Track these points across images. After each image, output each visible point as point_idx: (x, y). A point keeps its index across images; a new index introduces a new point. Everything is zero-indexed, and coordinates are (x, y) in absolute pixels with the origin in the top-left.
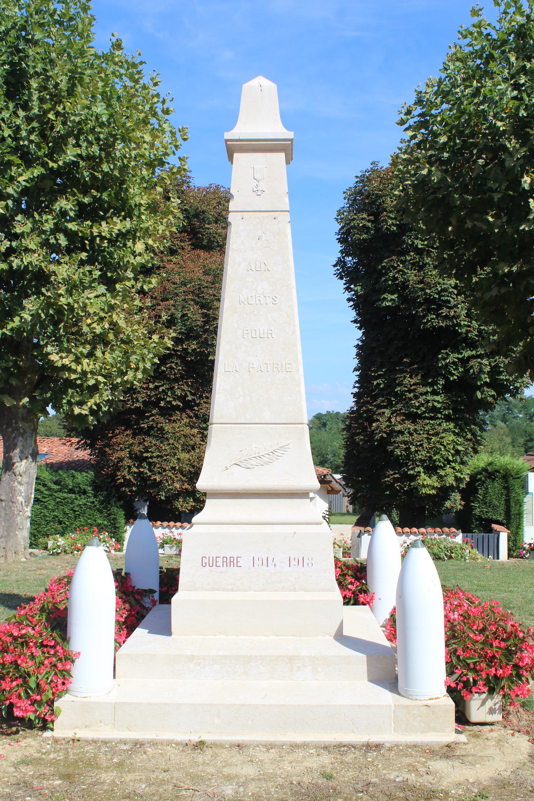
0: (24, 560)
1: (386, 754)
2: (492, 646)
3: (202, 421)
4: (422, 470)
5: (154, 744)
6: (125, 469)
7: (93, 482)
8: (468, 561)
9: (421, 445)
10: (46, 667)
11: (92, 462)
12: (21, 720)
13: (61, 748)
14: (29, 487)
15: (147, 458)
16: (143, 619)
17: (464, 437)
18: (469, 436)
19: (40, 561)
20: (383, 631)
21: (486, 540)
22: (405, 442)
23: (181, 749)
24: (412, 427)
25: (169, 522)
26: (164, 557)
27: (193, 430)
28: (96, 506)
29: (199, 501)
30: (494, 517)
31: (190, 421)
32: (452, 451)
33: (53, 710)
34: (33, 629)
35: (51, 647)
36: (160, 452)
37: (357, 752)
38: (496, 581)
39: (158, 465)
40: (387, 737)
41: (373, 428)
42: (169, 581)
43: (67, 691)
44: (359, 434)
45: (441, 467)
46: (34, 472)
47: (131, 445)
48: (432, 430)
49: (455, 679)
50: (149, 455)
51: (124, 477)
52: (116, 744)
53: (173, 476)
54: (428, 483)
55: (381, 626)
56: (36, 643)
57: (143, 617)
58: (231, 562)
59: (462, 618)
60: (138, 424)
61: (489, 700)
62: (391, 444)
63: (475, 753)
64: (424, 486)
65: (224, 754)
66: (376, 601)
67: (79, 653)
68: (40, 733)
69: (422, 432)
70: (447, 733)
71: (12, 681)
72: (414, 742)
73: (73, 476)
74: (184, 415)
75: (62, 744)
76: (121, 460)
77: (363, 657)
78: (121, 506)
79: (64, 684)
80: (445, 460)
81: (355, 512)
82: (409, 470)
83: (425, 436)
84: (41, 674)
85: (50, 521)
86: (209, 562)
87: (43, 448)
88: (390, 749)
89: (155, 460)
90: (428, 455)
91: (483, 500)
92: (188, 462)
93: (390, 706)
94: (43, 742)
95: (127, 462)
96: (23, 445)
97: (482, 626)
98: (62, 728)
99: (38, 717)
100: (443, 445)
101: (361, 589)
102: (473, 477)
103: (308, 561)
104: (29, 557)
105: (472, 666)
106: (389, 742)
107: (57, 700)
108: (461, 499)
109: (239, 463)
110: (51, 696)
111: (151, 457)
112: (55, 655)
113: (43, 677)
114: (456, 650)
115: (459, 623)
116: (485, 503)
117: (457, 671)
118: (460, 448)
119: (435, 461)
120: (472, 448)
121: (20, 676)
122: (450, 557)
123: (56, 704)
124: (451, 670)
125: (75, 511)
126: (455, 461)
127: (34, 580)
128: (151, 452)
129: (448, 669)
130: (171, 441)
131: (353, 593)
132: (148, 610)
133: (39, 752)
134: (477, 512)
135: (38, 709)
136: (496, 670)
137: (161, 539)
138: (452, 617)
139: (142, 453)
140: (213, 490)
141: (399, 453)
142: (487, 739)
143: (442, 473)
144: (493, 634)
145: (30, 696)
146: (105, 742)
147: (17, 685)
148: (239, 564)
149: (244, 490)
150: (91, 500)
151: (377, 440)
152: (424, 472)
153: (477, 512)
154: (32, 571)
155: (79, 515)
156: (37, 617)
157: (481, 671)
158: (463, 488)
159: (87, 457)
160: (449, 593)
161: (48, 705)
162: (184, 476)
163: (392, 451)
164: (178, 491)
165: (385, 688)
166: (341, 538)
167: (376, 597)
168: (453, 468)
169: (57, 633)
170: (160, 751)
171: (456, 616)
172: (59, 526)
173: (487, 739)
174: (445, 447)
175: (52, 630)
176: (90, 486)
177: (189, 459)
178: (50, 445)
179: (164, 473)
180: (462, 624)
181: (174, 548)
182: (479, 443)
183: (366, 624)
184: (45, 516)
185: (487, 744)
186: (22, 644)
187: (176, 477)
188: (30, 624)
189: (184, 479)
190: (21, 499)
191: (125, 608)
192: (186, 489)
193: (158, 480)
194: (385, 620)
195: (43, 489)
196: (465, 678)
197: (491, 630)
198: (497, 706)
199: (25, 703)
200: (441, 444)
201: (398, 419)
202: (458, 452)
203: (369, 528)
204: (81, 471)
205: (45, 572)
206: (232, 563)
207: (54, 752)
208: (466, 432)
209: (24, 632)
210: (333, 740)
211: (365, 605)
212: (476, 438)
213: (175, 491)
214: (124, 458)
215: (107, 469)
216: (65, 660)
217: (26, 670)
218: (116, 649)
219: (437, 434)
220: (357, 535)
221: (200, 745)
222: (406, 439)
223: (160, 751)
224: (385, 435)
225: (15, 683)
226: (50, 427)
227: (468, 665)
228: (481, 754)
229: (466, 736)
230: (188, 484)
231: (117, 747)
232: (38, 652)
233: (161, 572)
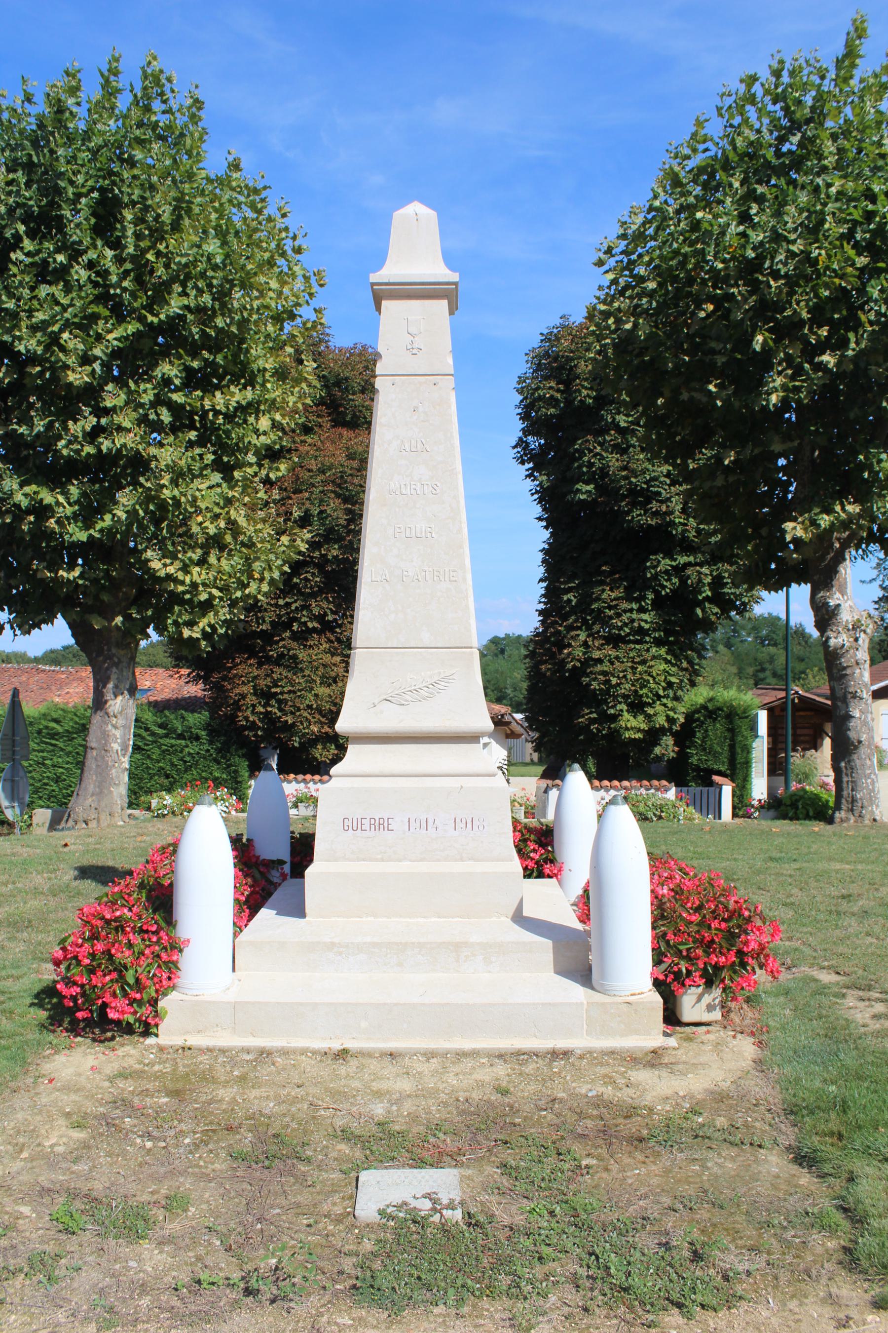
2: (709, 927)
4: (625, 708)
5: (285, 1052)
7: (208, 725)
9: (625, 676)
12: (118, 1023)
18: (685, 664)
19: (142, 825)
22: (604, 673)
24: (613, 653)
25: (304, 774)
29: (339, 745)
30: (715, 767)
32: (663, 684)
34: (130, 910)
35: (153, 933)
37: (540, 1061)
39: (290, 703)
40: (578, 1042)
42: (303, 849)
43: (174, 988)
44: (545, 662)
45: (649, 705)
47: (255, 678)
50: (278, 690)
51: (246, 718)
53: (309, 717)
54: (632, 725)
56: (134, 928)
57: (270, 894)
58: (380, 825)
64: (627, 729)
65: (373, 1065)
66: (565, 873)
67: (188, 941)
68: (141, 1040)
70: (652, 1035)
71: (105, 975)
73: (183, 717)
75: (169, 1053)
76: (243, 696)
77: (548, 943)
78: (244, 756)
79: (169, 978)
82: (609, 708)
83: (630, 664)
85: (154, 775)
86: (351, 825)
88: (581, 1057)
89: (286, 696)
93: (582, 1004)
95: (251, 699)
97: (697, 903)
98: (168, 1034)
102: (689, 717)
104: (127, 820)
105: (684, 953)
106: (580, 1048)
110: (154, 994)
111: (282, 693)
112: (158, 942)
114: (664, 935)
116: (704, 749)
118: (673, 679)
119: (641, 696)
122: (660, 818)
125: (185, 762)
130: (307, 672)
131: (537, 863)
132: (276, 886)
139: (270, 687)
143: (650, 711)
146: (223, 1051)
147: (111, 980)
150: (206, 747)
151: (569, 671)
152: (628, 711)
153: (694, 760)
156: (135, 896)
159: (200, 694)
160: (657, 862)
166: (522, 794)
167: (566, 868)
168: (665, 705)
171: (665, 891)
175: (154, 912)
182: (697, 673)
183: (552, 901)
184: (148, 768)
186: (116, 929)
189: (323, 720)
190: (116, 746)
192: (326, 733)
193: (290, 722)
195: (144, 734)
196: (676, 969)
198: (717, 1001)
199: (121, 1003)
202: (670, 685)
203: (558, 782)
207: (160, 1063)
209: (118, 913)
218: (235, 935)
219: (644, 662)
221: (343, 1054)
224: (578, 664)
225: (108, 978)
227: (681, 951)
228: (695, 1061)
232: (137, 939)
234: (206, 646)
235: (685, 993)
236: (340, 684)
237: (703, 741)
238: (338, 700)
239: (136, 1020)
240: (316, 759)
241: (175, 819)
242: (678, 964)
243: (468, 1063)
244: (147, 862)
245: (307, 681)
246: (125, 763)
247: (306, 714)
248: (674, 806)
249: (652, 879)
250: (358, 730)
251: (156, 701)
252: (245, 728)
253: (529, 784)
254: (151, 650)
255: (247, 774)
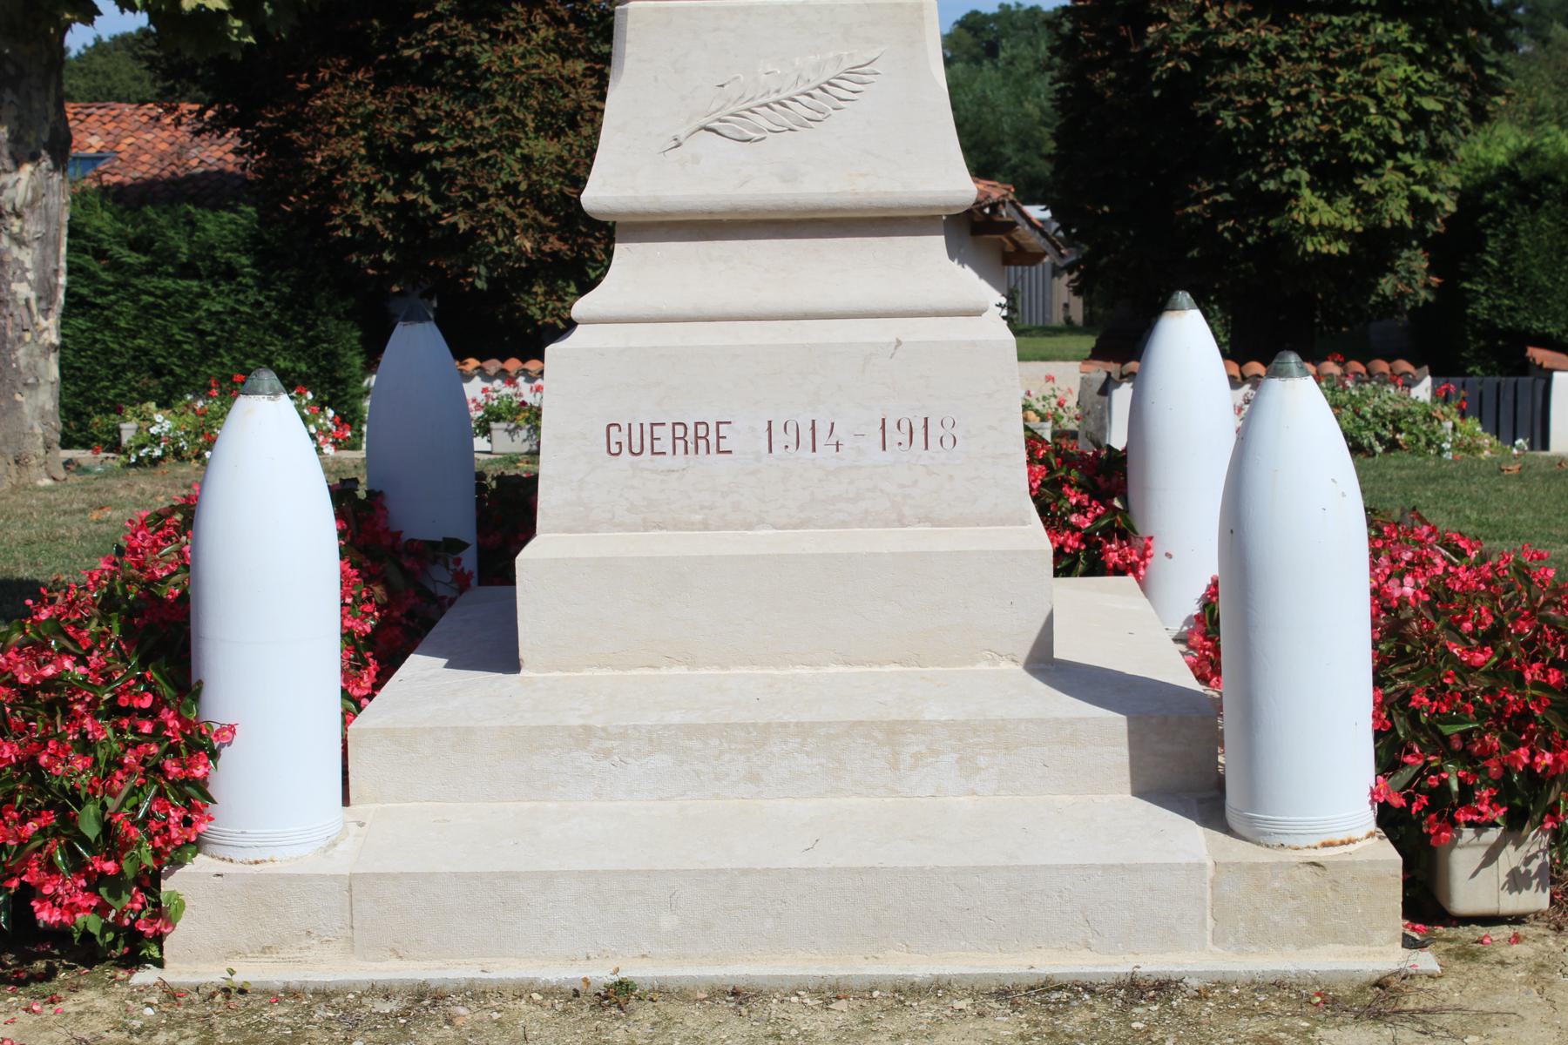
0: (48, 482)
1: (1188, 1010)
2: (1519, 681)
3: (597, 35)
4: (1305, 176)
5: (475, 993)
6: (354, 195)
7: (256, 239)
8: (1448, 456)
9: (1304, 96)
10: (131, 773)
11: (251, 176)
12: (59, 935)
13: (188, 1016)
14: (49, 250)
15: (426, 156)
16: (428, 629)
17: (1443, 69)
18: (1459, 65)
19: (99, 484)
20: (1183, 654)
21: (1507, 398)
22: (1248, 88)
23: (559, 1007)
24: (1272, 37)
26: (491, 462)
27: (569, 63)
28: (268, 315)
29: (584, 248)
30: (1535, 325)
31: (557, 35)
32: (1403, 115)
33: (158, 905)
34: (81, 660)
35: (143, 713)
36: (467, 138)
37: (1101, 1006)
38: (1537, 511)
39: (461, 180)
40: (1192, 960)
41: (1148, 43)
42: (509, 510)
43: (198, 845)
44: (1103, 64)
45: (1367, 169)
46: (60, 204)
47: (372, 117)
48: (1340, 45)
49: (1403, 783)
50: (431, 147)
51: (352, 221)
52: (359, 997)
53: (510, 214)
54: (1322, 218)
55: (1176, 640)
56: (92, 705)
57: (429, 624)
58: (700, 438)
59: (1427, 598)
60: (392, 49)
61: (1510, 848)
62: (1206, 94)
63: (1465, 1004)
64: (1310, 230)
65: (693, 1018)
66: (1157, 562)
67: (232, 729)
68: (121, 974)
69: (1305, 55)
70: (1379, 948)
71: (24, 820)
72: (1275, 973)
73: (191, 223)
74: (538, 18)
75: (191, 1003)
76: (340, 165)
77: (1117, 722)
78: (349, 315)
79: (187, 822)
80: (1379, 144)
81: (1089, 325)
82: (1264, 177)
83: (1315, 66)
84: (113, 795)
85: (124, 368)
86: (627, 441)
87: (88, 139)
88: (1201, 996)
89: (451, 162)
90: (1325, 128)
91: (1498, 271)
92: (556, 168)
93: (1202, 866)
94: (133, 999)
95: (361, 172)
96: (18, 118)
97: (1489, 621)
98: (192, 957)
99: (115, 927)
100: (1374, 96)
101: (1110, 525)
102: (1469, 198)
103: (941, 432)
104: (62, 474)
105: (1457, 745)
106: (1198, 975)
107: (170, 873)
108: (1430, 271)
109: (715, 125)
110: (149, 861)
111: (440, 155)
112: (156, 735)
113: (123, 804)
114: (1406, 696)
115: (1417, 611)
116: (1507, 281)
117: (1409, 759)
118: (1429, 104)
119: (1347, 147)
120: (1466, 104)
121: (50, 805)
122: (1392, 445)
123: (167, 886)
124: (1389, 754)
126: (1411, 148)
127: (83, 537)
128: (436, 137)
129: (1382, 753)
130: (501, 102)
131: (1087, 538)
132: (443, 605)
133: (120, 1027)
134: (1481, 308)
135: (109, 900)
136: (1532, 755)
137: (478, 407)
138: (1397, 593)
139: (409, 142)
140: (634, 214)
141: (1231, 124)
142: (1502, 963)
143: (1369, 186)
144: (1523, 644)
145: (86, 864)
146: (324, 995)
147: (42, 831)
148: (724, 445)
149: (735, 210)
150: (252, 295)
151: (1159, 83)
153: (1481, 308)
154: (72, 513)
155: (216, 345)
156: (93, 627)
157: (1486, 759)
158: (1436, 234)
159: (231, 162)
160: (1387, 530)
161: (142, 889)
162: (546, 213)
163: (1210, 117)
164: (528, 260)
165: (1187, 814)
166: (1047, 389)
167: (1157, 550)
168: (1406, 170)
169: (157, 670)
170: (496, 1016)
171: (1408, 590)
172: (154, 382)
173: (1502, 963)
174: (1379, 102)
175: (143, 664)
176: (247, 252)
177: (560, 158)
178: (110, 127)
179: (482, 206)
180: (1428, 614)
181: (523, 434)
182: (1490, 87)
183: (1130, 627)
184: (107, 351)
185: (1503, 976)
186: (50, 708)
187: (522, 216)
188: (71, 647)
189: (546, 221)
190: (23, 290)
191: (369, 599)
192: (554, 254)
193: (462, 227)
194: (1187, 622)
195: (95, 267)
196: (1433, 781)
197: (1520, 634)
198: (1534, 866)
199: (67, 886)
200: (1367, 93)
201: (1229, 12)
202: (1420, 117)
203: (1133, 366)
204: (214, 208)
205: (116, 514)
206: (702, 443)
207: (169, 1027)
208: (1448, 53)
209: (50, 671)
210: (1025, 970)
211: (1123, 573)
212: (1480, 72)
213: (519, 260)
214: (351, 160)
215: (298, 197)
216: (190, 752)
217: (68, 786)
218: (347, 717)
219: (1352, 61)
220: (1097, 387)
221: (619, 995)
222: (1253, 77)
223: (496, 1016)
224: (1186, 66)
225: (32, 826)
226: (107, 76)
227: (1446, 740)
228: (1484, 1007)
229: (1438, 956)
230: (560, 239)
231: (362, 1006)
232: (103, 732)
233: (481, 488)
234: (242, 32)
235: (1453, 844)
236: (587, 130)
237: (1504, 261)
238: (581, 171)
239: (106, 927)
240: (531, 320)
241: (183, 470)
242: (1438, 770)
243: (926, 1011)
244: (120, 551)
245: (502, 124)
246: (50, 330)
247: (501, 207)
248: (1429, 417)
249: (1373, 566)
250: (637, 206)
251: (120, 185)
252: (349, 245)
253: (1067, 378)
254: (99, 60)
255: (358, 361)
